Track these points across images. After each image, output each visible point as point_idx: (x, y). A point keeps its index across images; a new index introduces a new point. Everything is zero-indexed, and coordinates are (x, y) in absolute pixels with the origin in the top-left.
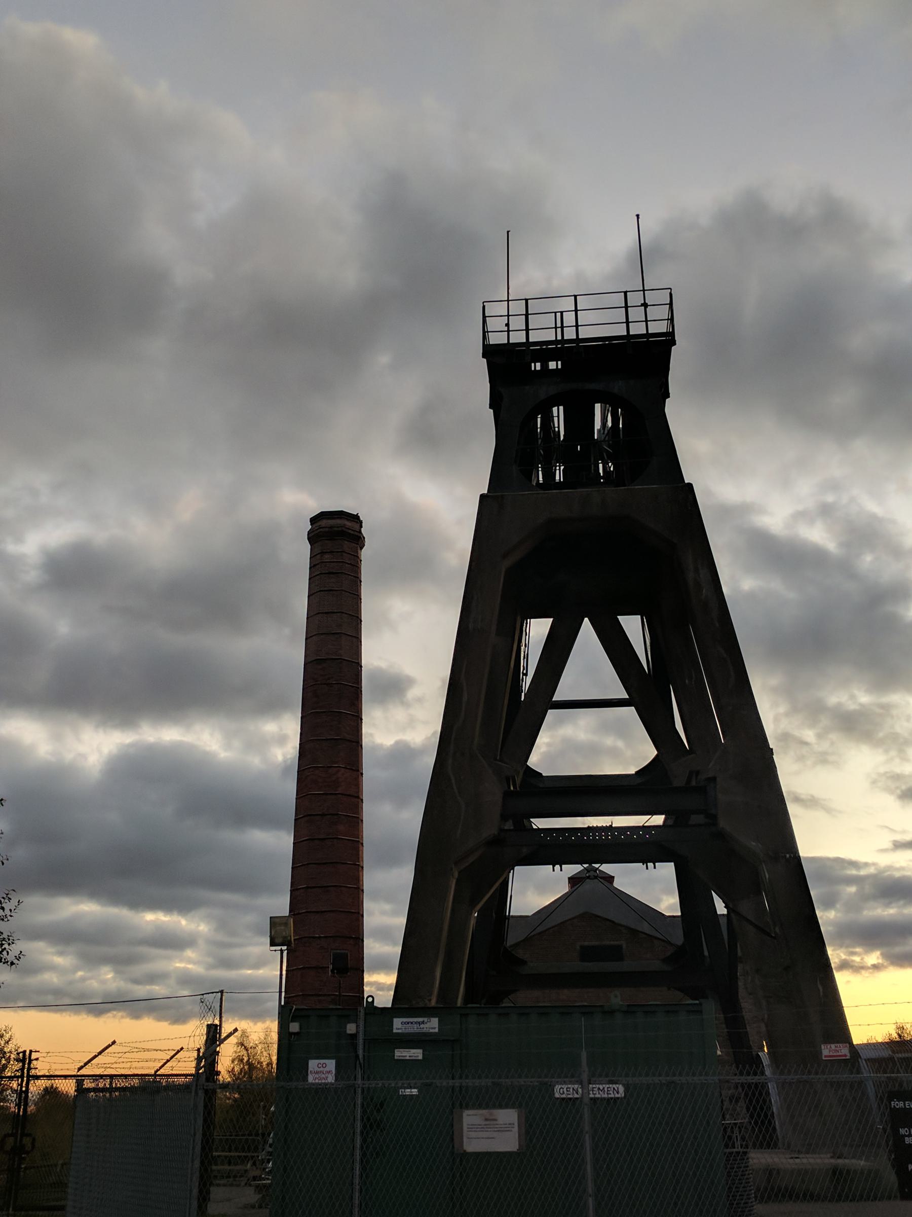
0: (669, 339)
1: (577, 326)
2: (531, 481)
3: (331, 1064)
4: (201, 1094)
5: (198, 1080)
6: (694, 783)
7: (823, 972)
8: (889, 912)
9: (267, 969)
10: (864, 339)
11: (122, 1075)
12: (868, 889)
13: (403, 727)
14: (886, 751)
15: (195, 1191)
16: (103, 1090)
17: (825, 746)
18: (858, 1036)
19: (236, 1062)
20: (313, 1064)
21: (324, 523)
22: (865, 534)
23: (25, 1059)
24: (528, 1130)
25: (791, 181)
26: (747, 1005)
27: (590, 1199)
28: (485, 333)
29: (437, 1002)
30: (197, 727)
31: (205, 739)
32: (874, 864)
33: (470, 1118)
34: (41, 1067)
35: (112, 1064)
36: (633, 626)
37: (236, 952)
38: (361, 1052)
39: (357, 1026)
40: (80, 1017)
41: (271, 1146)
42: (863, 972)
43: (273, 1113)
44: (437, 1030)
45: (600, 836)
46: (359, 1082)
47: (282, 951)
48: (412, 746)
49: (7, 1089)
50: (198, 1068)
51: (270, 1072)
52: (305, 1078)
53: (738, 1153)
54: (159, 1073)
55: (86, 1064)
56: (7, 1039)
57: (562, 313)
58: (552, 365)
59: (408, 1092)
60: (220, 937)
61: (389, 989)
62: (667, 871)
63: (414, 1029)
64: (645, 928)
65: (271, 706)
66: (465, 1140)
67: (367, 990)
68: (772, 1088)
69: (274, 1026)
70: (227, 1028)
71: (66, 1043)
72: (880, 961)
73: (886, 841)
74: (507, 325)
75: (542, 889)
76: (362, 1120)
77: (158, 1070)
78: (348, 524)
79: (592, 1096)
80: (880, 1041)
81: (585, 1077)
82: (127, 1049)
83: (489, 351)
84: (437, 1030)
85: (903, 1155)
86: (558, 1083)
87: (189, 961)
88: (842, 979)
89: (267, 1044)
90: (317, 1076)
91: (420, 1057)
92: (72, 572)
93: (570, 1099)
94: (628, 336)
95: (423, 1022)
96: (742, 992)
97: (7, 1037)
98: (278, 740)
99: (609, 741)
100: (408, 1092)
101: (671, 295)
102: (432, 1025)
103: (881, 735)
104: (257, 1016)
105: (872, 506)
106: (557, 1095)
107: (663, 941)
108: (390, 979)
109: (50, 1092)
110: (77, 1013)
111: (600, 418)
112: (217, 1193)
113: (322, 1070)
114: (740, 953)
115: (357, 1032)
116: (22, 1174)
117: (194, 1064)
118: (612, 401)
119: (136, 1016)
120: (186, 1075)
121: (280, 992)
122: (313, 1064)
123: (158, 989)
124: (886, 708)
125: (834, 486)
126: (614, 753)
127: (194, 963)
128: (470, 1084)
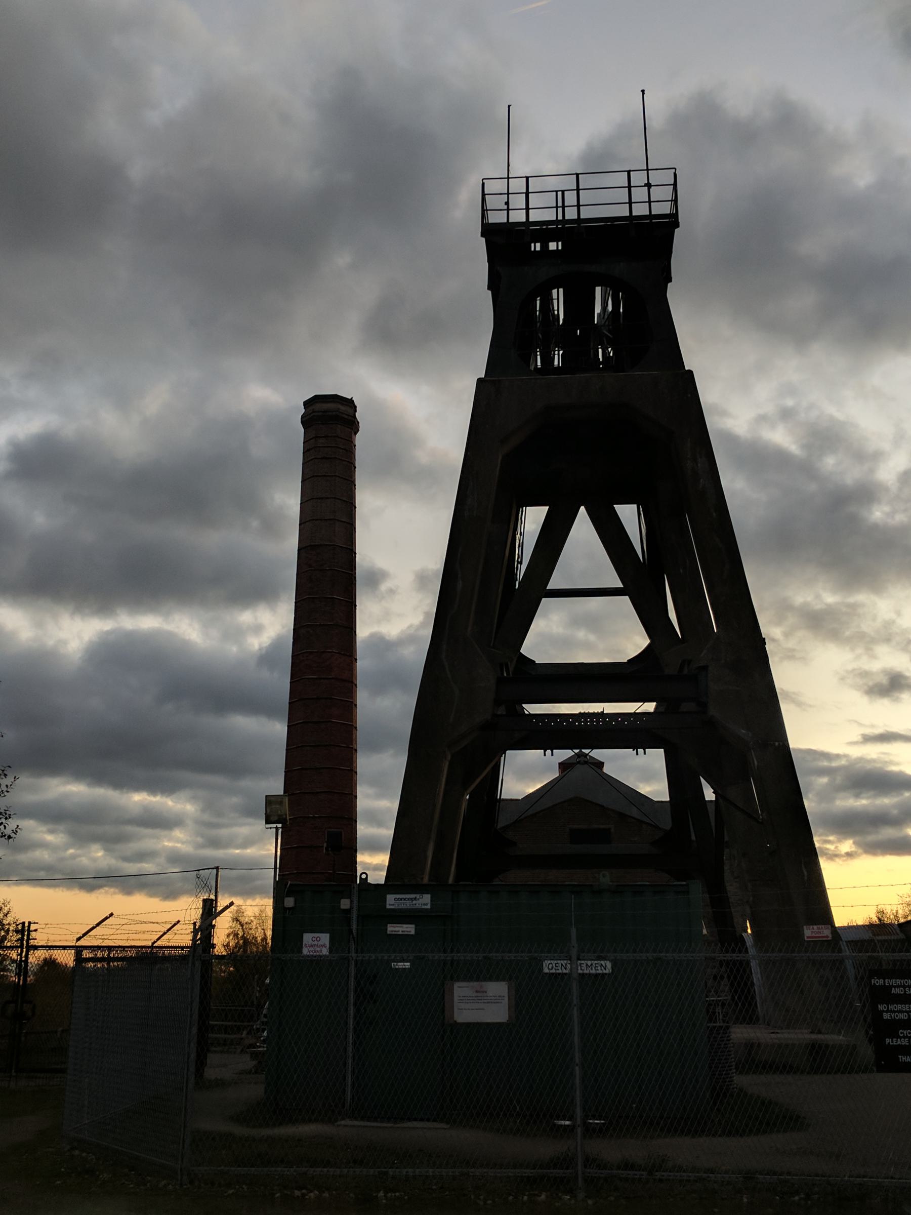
0: (672, 221)
1: (578, 206)
2: (529, 366)
3: (325, 938)
4: (198, 964)
5: (195, 951)
6: (686, 671)
7: (810, 856)
8: (863, 803)
9: (263, 847)
10: (817, 244)
11: (119, 947)
12: (839, 780)
13: (396, 613)
14: (852, 649)
15: (193, 1056)
16: (102, 959)
17: (791, 644)
18: (841, 918)
19: (231, 937)
20: (307, 938)
21: (318, 406)
22: (825, 437)
23: (24, 930)
24: (518, 1003)
25: (745, 83)
26: (732, 889)
27: (577, 1068)
28: (484, 211)
29: (430, 880)
30: (177, 617)
31: (185, 628)
32: (845, 756)
33: (461, 991)
34: (39, 938)
35: (106, 936)
36: (628, 515)
37: (224, 832)
38: (354, 927)
39: (352, 902)
40: (73, 892)
41: (265, 1016)
42: (837, 860)
43: (268, 985)
44: (429, 907)
45: (592, 721)
46: (354, 955)
47: (277, 828)
48: (387, 638)
49: (5, 960)
50: (194, 940)
51: (265, 947)
52: (300, 950)
53: (721, 1027)
54: (156, 945)
55: (85, 935)
56: (5, 912)
57: (563, 192)
58: (552, 246)
59: (401, 965)
60: (206, 817)
61: (381, 870)
62: (656, 758)
63: (407, 905)
64: (634, 812)
65: (253, 591)
66: (456, 1010)
67: (359, 870)
68: (753, 964)
69: (270, 902)
70: (222, 902)
71: (61, 917)
72: (853, 849)
73: (855, 734)
74: (507, 203)
75: (525, 774)
76: (355, 991)
77: (155, 942)
78: (342, 408)
79: (580, 971)
80: (860, 923)
81: (574, 953)
82: (126, 921)
83: (489, 231)
84: (429, 907)
85: (881, 1029)
86: (547, 958)
87: (178, 840)
88: (824, 864)
89: (260, 917)
90: (311, 949)
91: (413, 933)
92: (39, 463)
93: (559, 974)
95: (415, 899)
96: (727, 875)
97: (5, 910)
98: (272, 624)
99: (581, 634)
100: (401, 965)
101: (675, 175)
102: (424, 901)
103: (847, 633)
104: (249, 892)
105: (832, 410)
106: (546, 970)
107: (651, 825)
108: (383, 859)
109: (50, 963)
110: (69, 887)
111: (601, 303)
112: (213, 1058)
113: (316, 943)
114: (726, 839)
115: (351, 908)
116: (23, 1039)
117: (190, 937)
118: (613, 285)
119: (128, 892)
120: (182, 948)
121: (275, 868)
122: (307, 938)
123: (148, 867)
124: (854, 607)
125: (790, 390)
126: (587, 646)
127: (183, 843)
128: (462, 958)
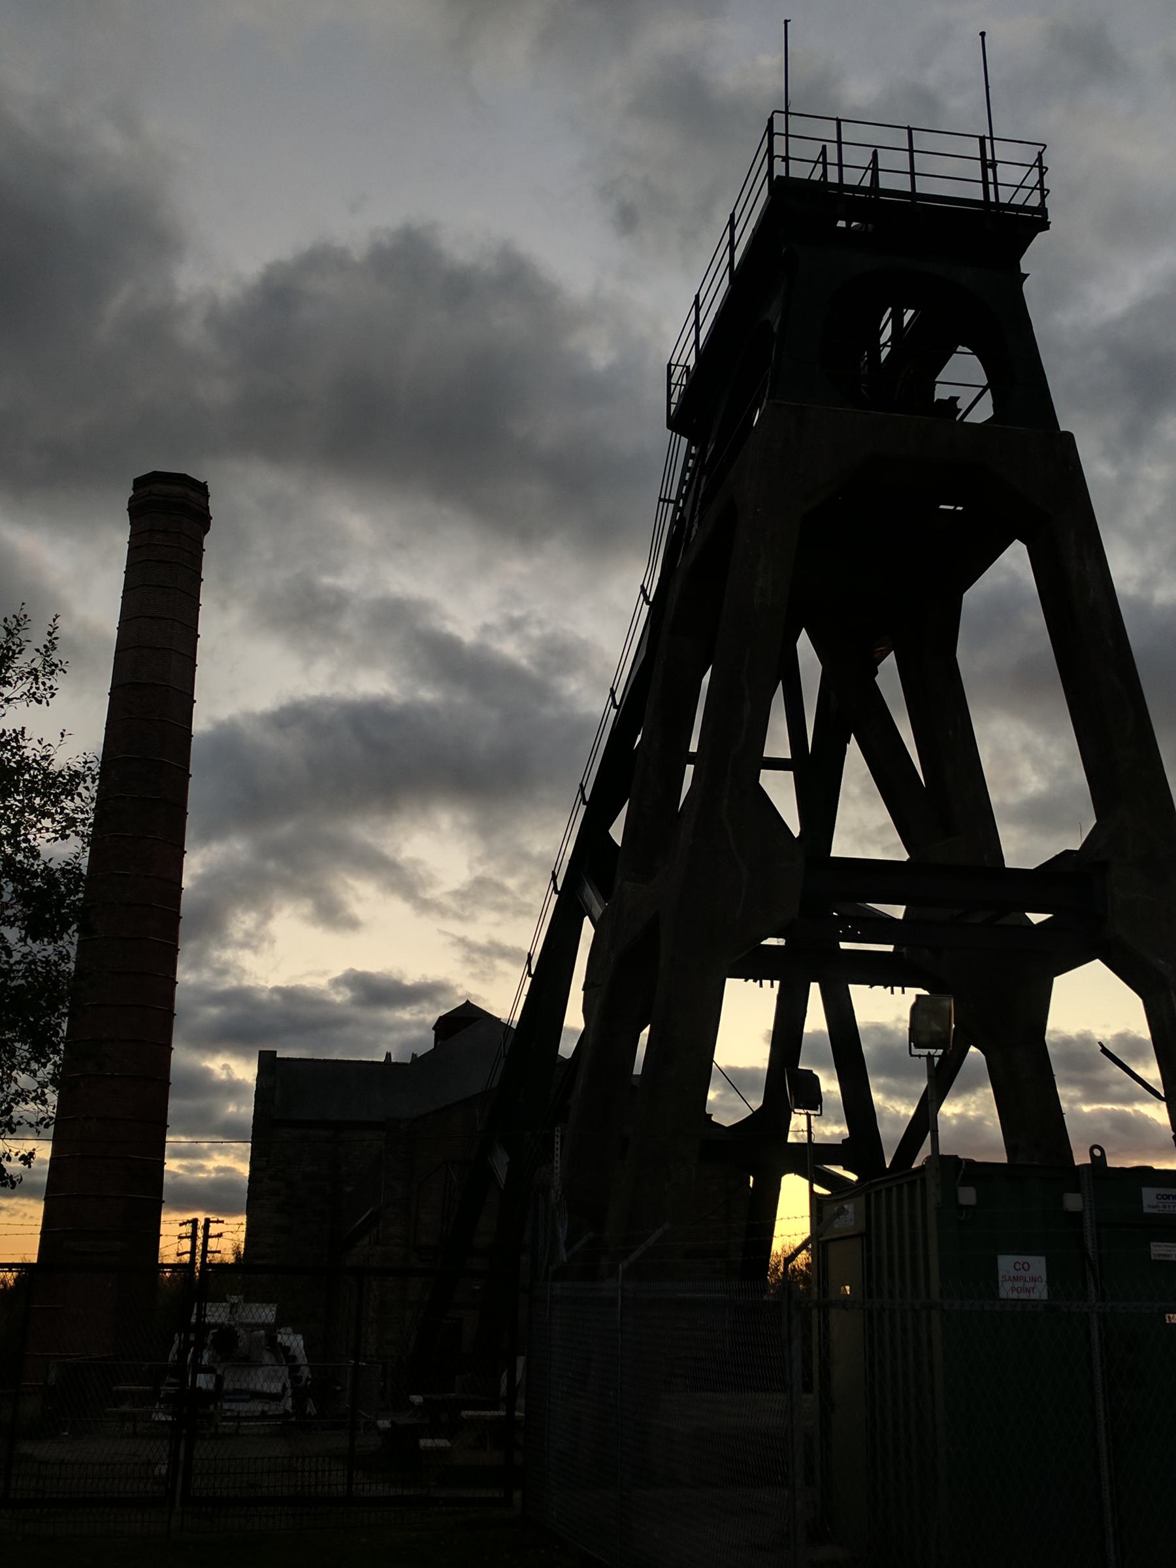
3: (1038, 1265)
20: (1006, 1264)
38: (1090, 1244)
94: (913, 195)
122: (1006, 1264)
